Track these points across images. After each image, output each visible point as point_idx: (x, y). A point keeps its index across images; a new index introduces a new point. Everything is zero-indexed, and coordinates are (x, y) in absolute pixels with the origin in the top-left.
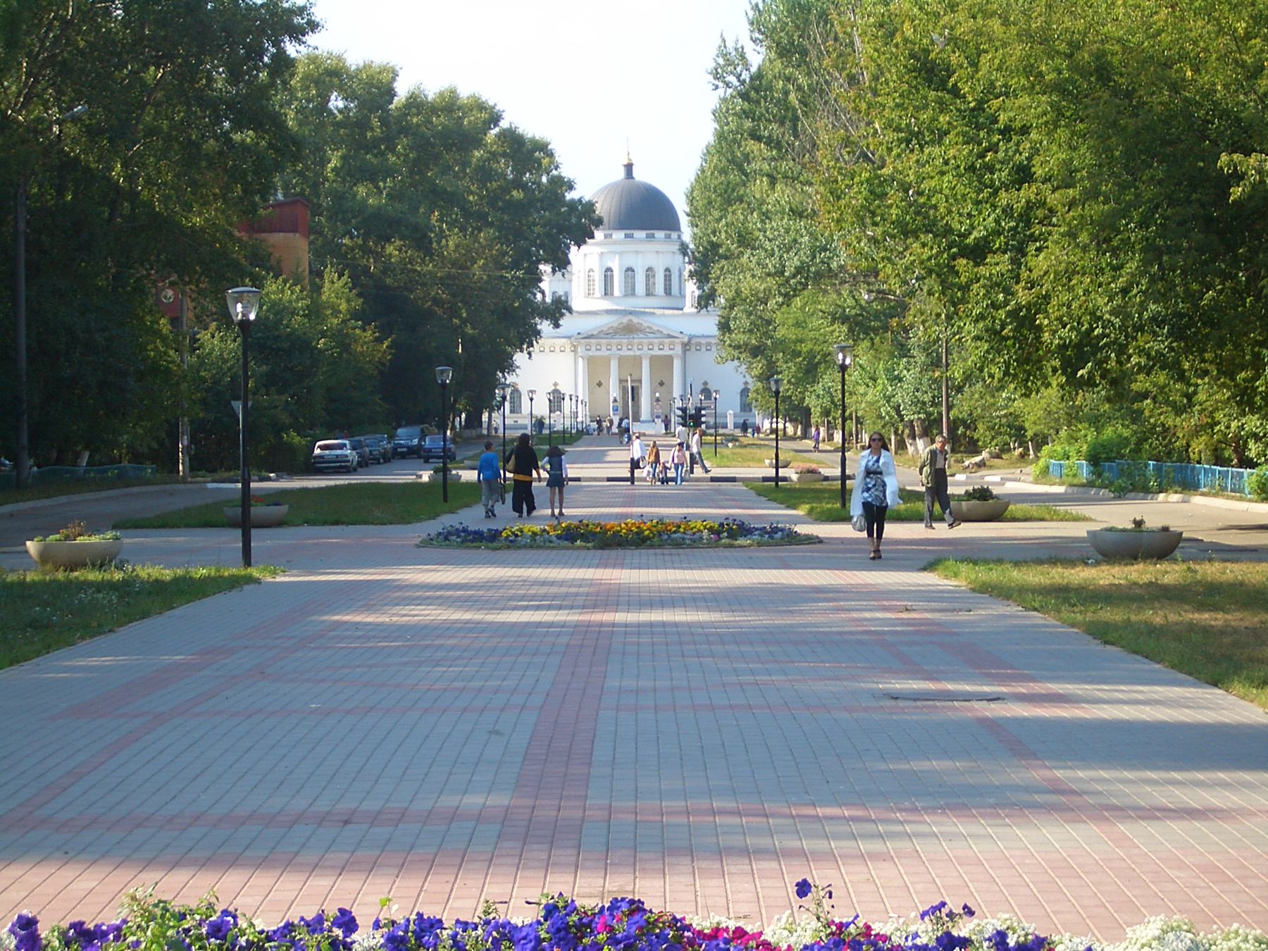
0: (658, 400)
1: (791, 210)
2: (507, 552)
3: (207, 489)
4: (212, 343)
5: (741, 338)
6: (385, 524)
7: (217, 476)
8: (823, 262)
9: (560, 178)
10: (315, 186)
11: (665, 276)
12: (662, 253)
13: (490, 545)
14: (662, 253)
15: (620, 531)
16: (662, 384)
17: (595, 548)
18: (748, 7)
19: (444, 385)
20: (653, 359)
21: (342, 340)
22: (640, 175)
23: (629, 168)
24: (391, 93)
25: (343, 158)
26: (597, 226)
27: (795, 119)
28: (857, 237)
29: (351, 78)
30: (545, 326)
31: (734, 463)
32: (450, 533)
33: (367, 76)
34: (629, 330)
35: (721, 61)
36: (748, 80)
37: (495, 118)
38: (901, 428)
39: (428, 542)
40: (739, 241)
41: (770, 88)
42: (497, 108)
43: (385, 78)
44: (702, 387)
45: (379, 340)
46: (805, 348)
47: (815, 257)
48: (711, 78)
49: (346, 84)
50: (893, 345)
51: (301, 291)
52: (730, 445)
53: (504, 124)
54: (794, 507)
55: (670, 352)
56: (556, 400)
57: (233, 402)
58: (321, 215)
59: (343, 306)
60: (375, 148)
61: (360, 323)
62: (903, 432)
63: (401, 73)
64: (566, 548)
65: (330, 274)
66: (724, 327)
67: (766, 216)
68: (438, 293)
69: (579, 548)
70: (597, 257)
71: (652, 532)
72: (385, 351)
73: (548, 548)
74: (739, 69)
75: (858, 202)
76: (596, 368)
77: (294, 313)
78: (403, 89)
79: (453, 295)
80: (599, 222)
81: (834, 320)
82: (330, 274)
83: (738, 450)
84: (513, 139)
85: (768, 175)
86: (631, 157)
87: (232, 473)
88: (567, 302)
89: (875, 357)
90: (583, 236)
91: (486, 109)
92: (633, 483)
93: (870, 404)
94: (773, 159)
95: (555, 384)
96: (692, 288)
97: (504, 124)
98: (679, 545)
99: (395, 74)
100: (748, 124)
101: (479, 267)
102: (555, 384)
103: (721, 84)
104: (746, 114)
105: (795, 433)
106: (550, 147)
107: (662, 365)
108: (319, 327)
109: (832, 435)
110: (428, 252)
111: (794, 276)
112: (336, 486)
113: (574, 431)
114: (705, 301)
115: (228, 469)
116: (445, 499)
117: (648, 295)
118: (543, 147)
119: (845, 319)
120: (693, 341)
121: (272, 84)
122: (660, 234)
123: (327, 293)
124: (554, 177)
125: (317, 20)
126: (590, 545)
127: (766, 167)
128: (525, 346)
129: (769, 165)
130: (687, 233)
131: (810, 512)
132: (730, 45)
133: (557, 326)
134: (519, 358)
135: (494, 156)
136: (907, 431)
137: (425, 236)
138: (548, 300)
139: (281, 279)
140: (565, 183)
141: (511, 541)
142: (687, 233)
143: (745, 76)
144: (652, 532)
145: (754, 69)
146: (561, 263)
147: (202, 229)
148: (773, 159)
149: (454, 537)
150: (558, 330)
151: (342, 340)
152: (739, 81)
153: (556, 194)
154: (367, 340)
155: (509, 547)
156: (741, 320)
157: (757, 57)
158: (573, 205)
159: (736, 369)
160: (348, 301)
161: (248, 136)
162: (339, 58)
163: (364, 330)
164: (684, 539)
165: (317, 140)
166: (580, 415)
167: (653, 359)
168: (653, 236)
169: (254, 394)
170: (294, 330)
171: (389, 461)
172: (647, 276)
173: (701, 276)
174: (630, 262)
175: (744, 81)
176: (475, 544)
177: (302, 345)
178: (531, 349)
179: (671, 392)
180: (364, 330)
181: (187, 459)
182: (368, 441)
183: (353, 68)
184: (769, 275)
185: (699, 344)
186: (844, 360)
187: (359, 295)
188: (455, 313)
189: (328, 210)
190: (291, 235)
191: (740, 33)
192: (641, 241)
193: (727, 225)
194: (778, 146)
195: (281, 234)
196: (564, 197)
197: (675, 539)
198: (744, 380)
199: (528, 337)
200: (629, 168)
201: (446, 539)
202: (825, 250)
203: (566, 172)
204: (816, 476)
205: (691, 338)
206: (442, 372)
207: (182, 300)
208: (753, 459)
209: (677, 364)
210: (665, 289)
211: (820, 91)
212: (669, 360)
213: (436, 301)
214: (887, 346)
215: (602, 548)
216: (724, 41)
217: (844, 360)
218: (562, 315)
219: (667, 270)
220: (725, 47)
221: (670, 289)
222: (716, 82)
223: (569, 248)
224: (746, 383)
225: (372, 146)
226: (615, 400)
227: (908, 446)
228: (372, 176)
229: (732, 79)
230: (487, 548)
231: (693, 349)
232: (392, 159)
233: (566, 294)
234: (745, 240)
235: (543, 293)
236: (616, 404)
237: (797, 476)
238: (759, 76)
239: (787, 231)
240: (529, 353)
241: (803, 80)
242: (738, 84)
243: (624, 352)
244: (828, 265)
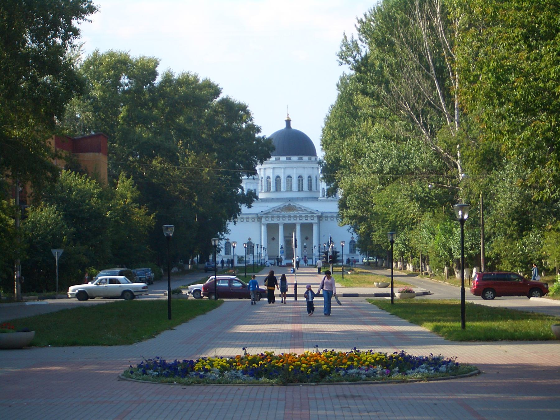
0: (305, 247)
1: (385, 136)
2: (196, 388)
3: (25, 305)
4: (41, 214)
5: (352, 212)
6: (112, 345)
7: (42, 295)
8: (405, 165)
9: (253, 125)
10: (112, 127)
11: (308, 180)
12: (306, 168)
13: (182, 380)
14: (306, 168)
15: (300, 366)
16: (273, 239)
17: (277, 384)
18: (356, 22)
19: (169, 237)
20: (302, 225)
21: (125, 213)
22: (294, 126)
23: (288, 122)
24: (154, 74)
25: (128, 111)
26: (272, 151)
27: (387, 82)
28: (488, 114)
29: (133, 65)
30: (244, 208)
31: (356, 285)
32: (148, 367)
33: (141, 64)
34: (289, 208)
35: (344, 49)
36: (360, 60)
37: (217, 92)
38: (451, 263)
39: (129, 374)
40: (355, 154)
41: (373, 65)
42: (219, 87)
43: (151, 64)
44: (351, 240)
45: (149, 214)
46: (392, 218)
47: (400, 162)
48: (338, 58)
49: (130, 69)
50: (445, 214)
51: (96, 183)
52: (349, 273)
53: (222, 96)
54: (418, 322)
55: (294, 222)
56: (250, 247)
57: (52, 250)
58: (115, 143)
59: (129, 195)
60: (146, 105)
61: (138, 204)
62: (453, 265)
63: (160, 62)
64: (252, 384)
65: (122, 176)
66: (343, 205)
67: (370, 140)
68: (182, 188)
69: (263, 384)
70: (271, 170)
71: (329, 367)
72: (152, 220)
73: (235, 384)
74: (354, 53)
75: (489, 85)
76: (272, 229)
77: (92, 196)
78: (161, 70)
79: (191, 188)
80: (273, 149)
81: (412, 199)
82: (122, 176)
83: (354, 276)
84: (227, 104)
85: (371, 116)
86: (289, 116)
87: (51, 293)
88: (255, 193)
89: (435, 222)
90: (264, 157)
91: (212, 87)
92: (296, 299)
93: (433, 248)
94: (374, 106)
95: (250, 239)
96: (323, 185)
97: (222, 96)
98: (355, 380)
99: (157, 64)
100: (360, 85)
101: (206, 173)
102: (250, 239)
103: (344, 62)
104: (359, 80)
105: (382, 265)
106: (248, 109)
107: (307, 228)
108: (107, 205)
109: (406, 266)
110: (177, 164)
111: (388, 173)
112: (107, 303)
113: (259, 264)
114: (331, 192)
115: (48, 291)
116: (170, 318)
117: (299, 191)
118: (244, 108)
119: (418, 199)
120: (324, 215)
121: (64, 45)
122: (305, 158)
123: (120, 188)
124: (249, 125)
125: (95, 5)
126: (274, 381)
127: (369, 112)
128: (232, 218)
129: (372, 110)
130: (320, 154)
131: (437, 330)
132: (349, 39)
133: (250, 207)
134: (230, 225)
135: (216, 112)
136: (455, 265)
137: (174, 155)
138: (245, 193)
139: (84, 176)
140: (255, 128)
141: (201, 377)
142: (320, 154)
143: (358, 58)
144: (329, 367)
145: (363, 54)
146: (252, 172)
147: (21, 139)
148: (374, 106)
149: (151, 371)
150: (250, 209)
151: (125, 213)
152: (355, 60)
153: (250, 135)
154: (141, 214)
155: (199, 383)
156: (352, 201)
157: (365, 49)
158: (259, 140)
159: (349, 230)
160: (132, 192)
161: (47, 79)
162: (126, 55)
163: (140, 208)
164: (359, 374)
165: (113, 100)
166: (263, 255)
167: (302, 225)
169: (67, 245)
170: (92, 207)
171: (152, 284)
172: (299, 181)
173: (329, 179)
174: (289, 172)
175: (358, 60)
176: (169, 379)
177: (97, 215)
178: (236, 220)
179: (312, 243)
180: (140, 208)
181: (19, 285)
182: (138, 273)
183: (134, 60)
184: (374, 173)
185: (327, 217)
186: (463, 216)
187: (138, 189)
188: (191, 197)
189: (119, 140)
190: (97, 154)
191: (353, 34)
192: (295, 162)
193: (348, 145)
194: (378, 98)
195: (92, 154)
196: (255, 136)
197: (352, 374)
198: (352, 236)
199: (234, 213)
200: (288, 122)
201: (144, 372)
202: (406, 158)
203: (257, 122)
204: (412, 294)
205: (322, 213)
206: (167, 228)
207: (16, 187)
208: (365, 282)
209: (315, 228)
210: (308, 187)
211: (400, 66)
212: (311, 226)
213: (182, 192)
214: (442, 215)
215: (284, 384)
216: (346, 37)
217: (463, 216)
218: (253, 201)
219: (310, 177)
220: (347, 41)
221: (311, 187)
222: (341, 61)
223: (256, 164)
224: (352, 238)
225: (144, 105)
226: (282, 248)
227: (456, 273)
228: (145, 121)
229: (350, 59)
230: (179, 383)
231: (324, 219)
232: (155, 112)
233: (255, 190)
234: (358, 154)
235: (242, 188)
236: (283, 249)
237: (399, 294)
238: (366, 58)
239: (384, 147)
240: (235, 222)
241: (393, 60)
242: (354, 62)
243: (270, 221)
244: (408, 167)
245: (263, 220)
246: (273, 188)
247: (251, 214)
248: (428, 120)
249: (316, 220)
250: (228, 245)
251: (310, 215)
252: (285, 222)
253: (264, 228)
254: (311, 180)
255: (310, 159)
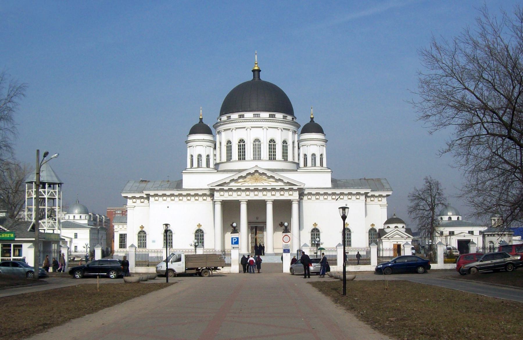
11: (283, 146)
20: (276, 203)
22: (264, 77)
44: (140, 230)
95: (199, 225)
102: (142, 227)
117: (270, 159)
122: (279, 116)
168: (274, 116)
192: (265, 120)
212: (288, 204)
219: (285, 142)
245: (218, 196)
246: (279, 155)
247: (201, 189)
248: (511, 91)
249: (295, 196)
250: (199, 233)
251: (287, 188)
252: (249, 198)
253: (218, 207)
254: (231, 146)
255: (285, 117)
